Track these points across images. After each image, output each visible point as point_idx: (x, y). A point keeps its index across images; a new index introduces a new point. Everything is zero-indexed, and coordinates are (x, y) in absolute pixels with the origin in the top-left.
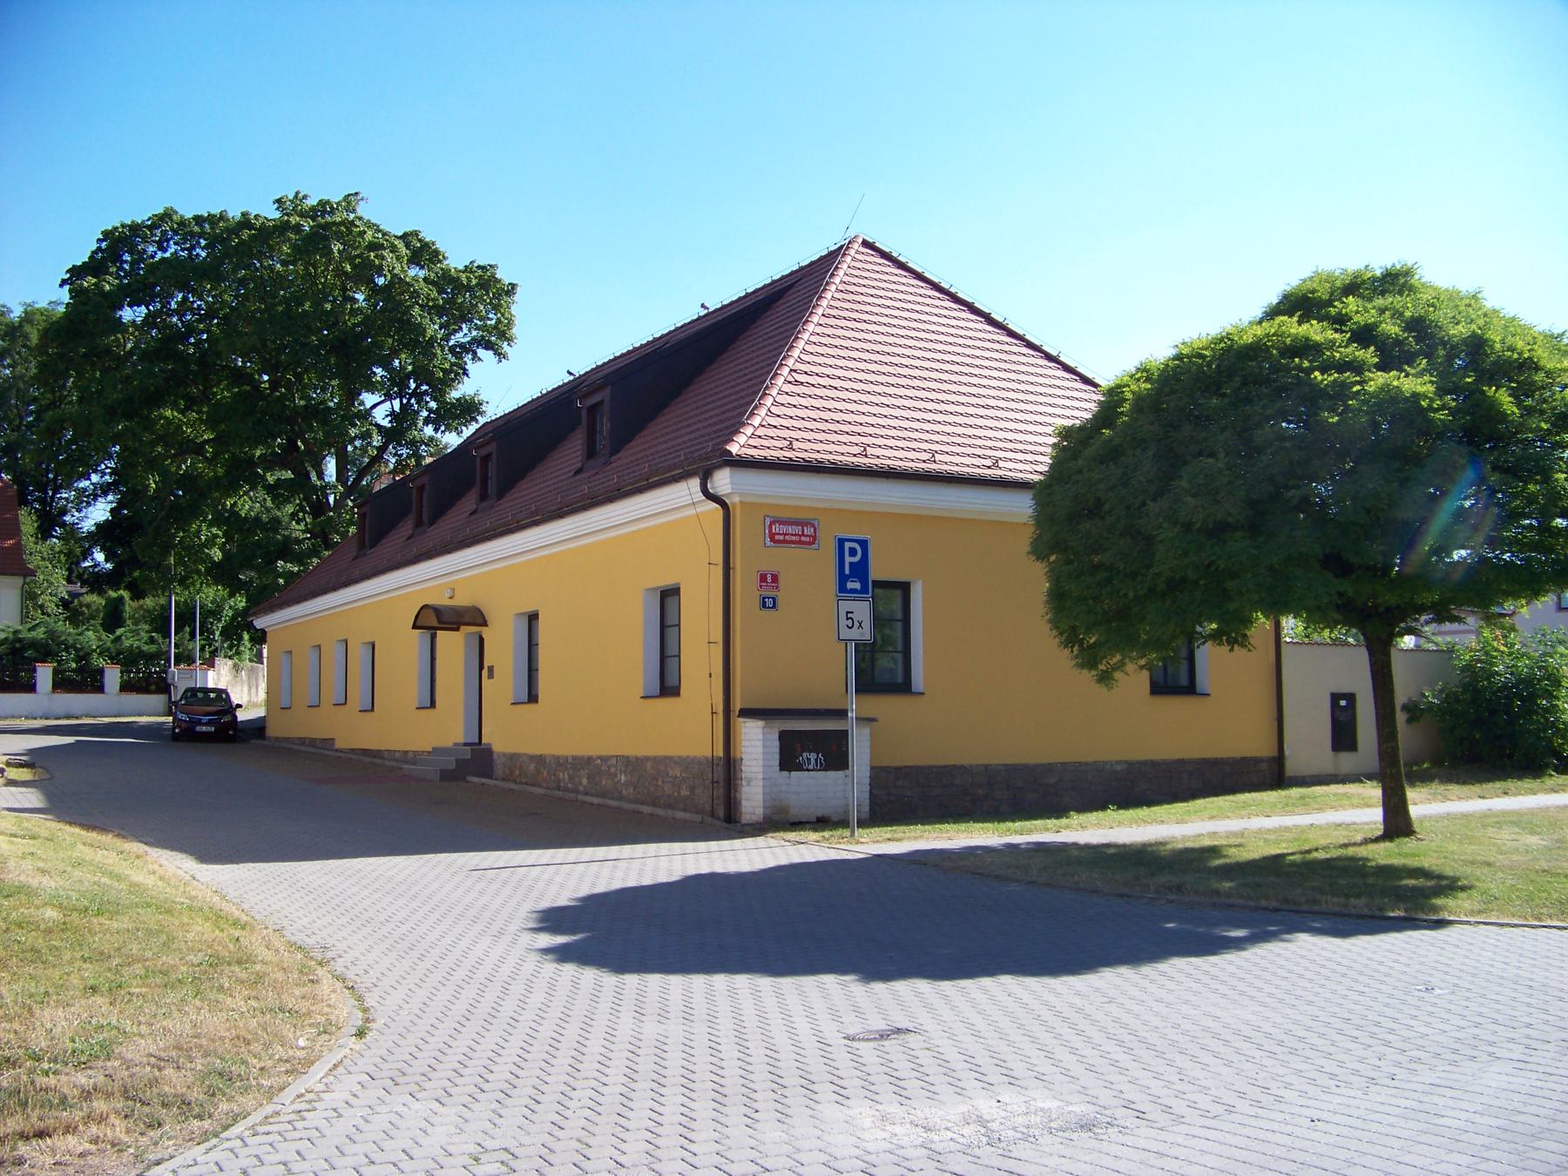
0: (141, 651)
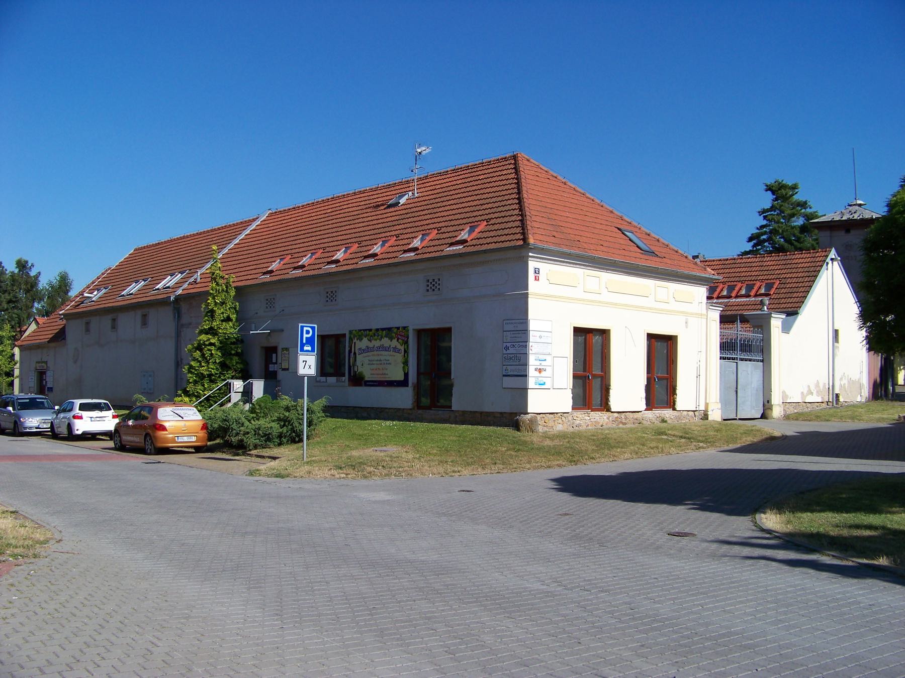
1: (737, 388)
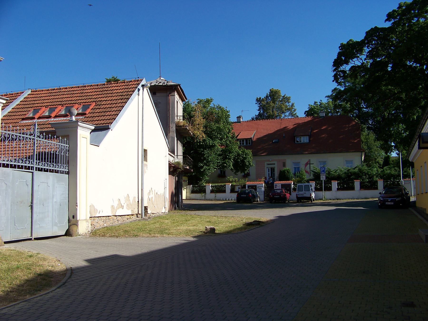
0: (392, 175)
1: (32, 203)
